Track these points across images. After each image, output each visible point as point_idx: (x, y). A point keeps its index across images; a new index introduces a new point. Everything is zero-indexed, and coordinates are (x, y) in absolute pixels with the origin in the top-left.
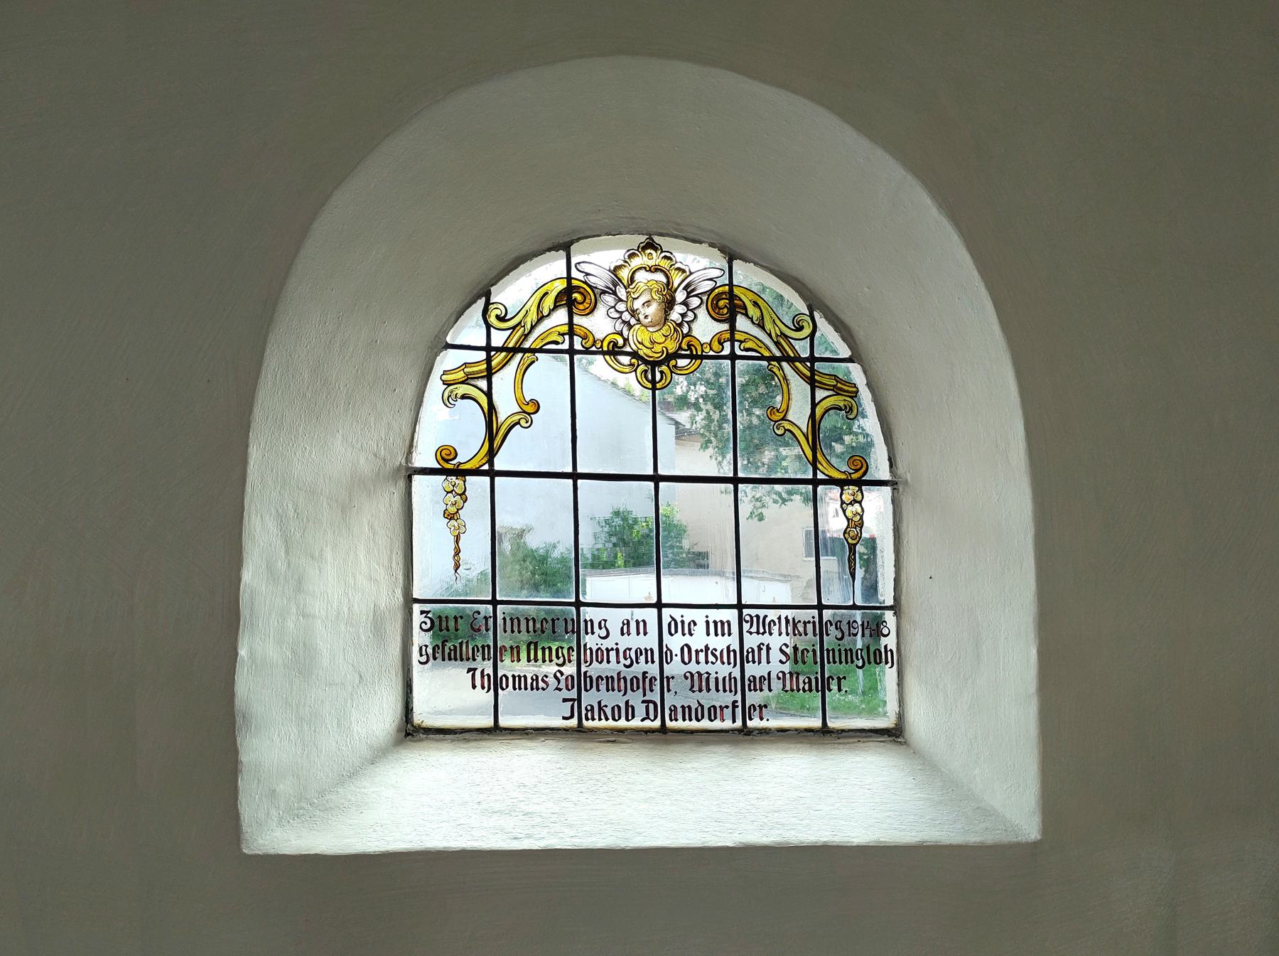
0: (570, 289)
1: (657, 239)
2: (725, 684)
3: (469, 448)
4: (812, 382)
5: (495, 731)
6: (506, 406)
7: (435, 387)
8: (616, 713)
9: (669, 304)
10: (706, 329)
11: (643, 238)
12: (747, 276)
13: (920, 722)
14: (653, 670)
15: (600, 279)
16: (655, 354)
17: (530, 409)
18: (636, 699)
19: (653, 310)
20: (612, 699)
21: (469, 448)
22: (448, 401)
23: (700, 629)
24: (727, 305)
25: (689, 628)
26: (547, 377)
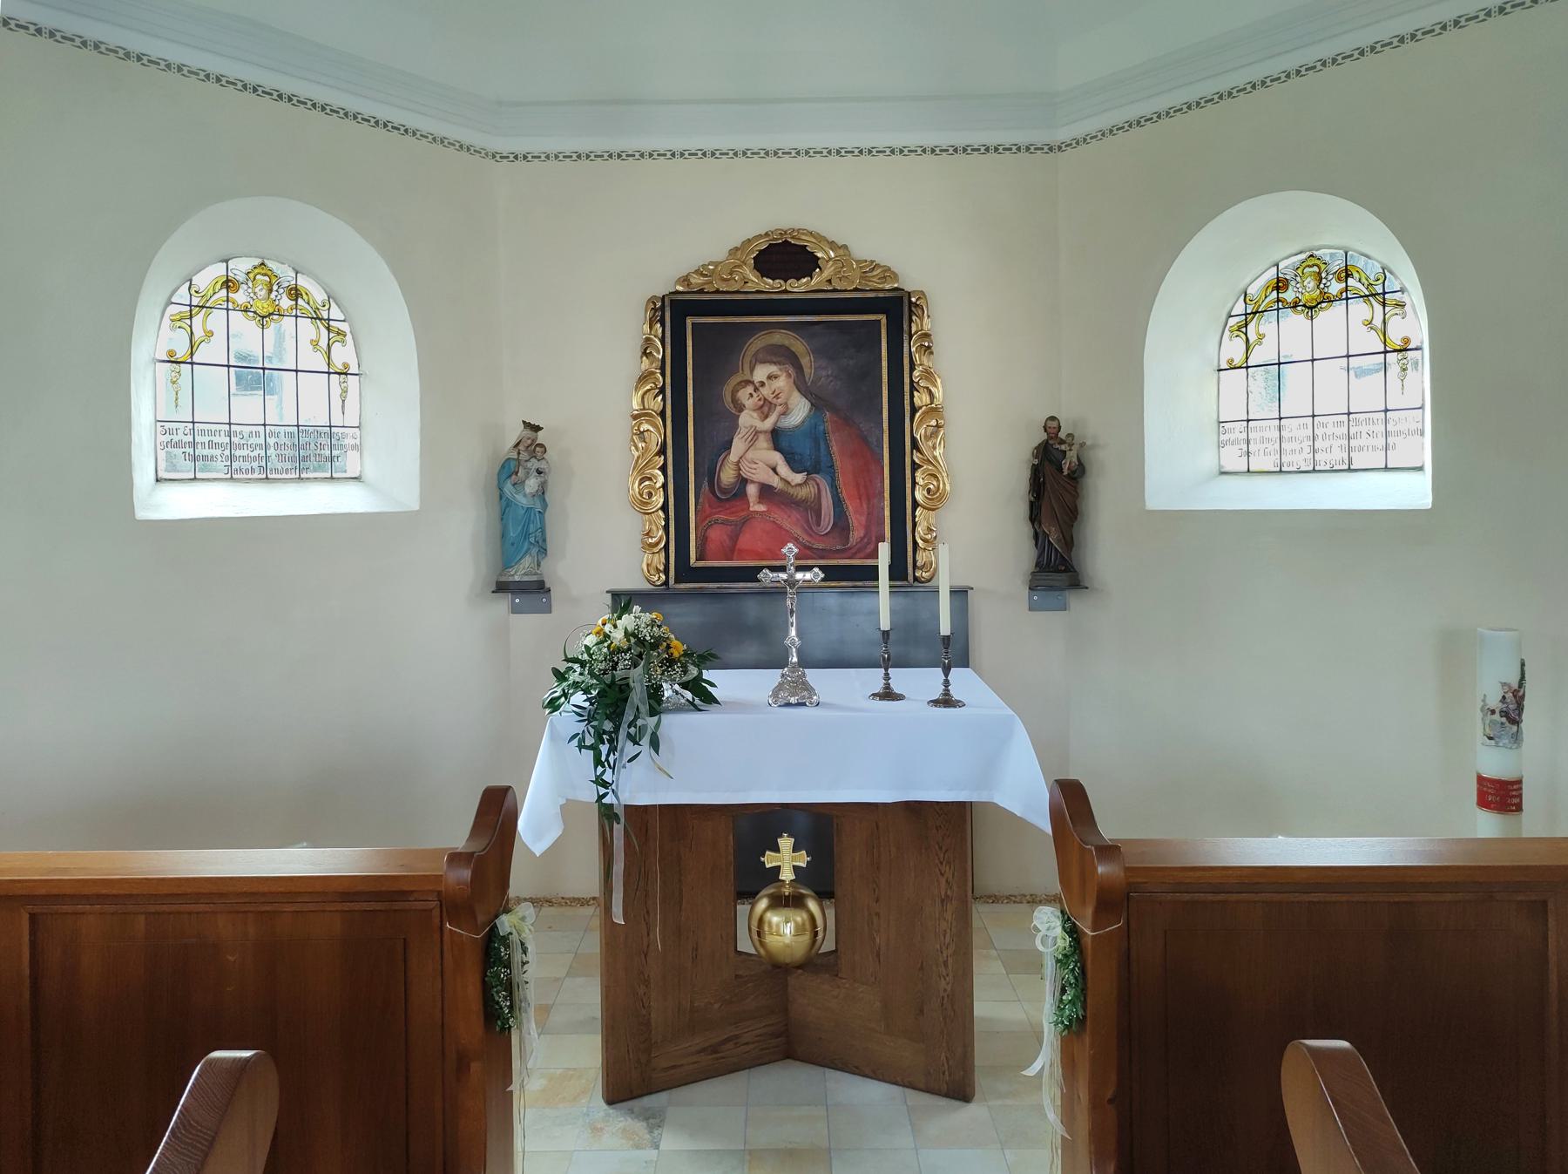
0: (228, 281)
1: (269, 264)
2: (291, 459)
3: (182, 352)
4: (328, 329)
5: (195, 479)
6: (199, 333)
7: (166, 321)
8: (247, 472)
9: (271, 291)
10: (286, 303)
11: (257, 262)
12: (304, 282)
13: (369, 473)
14: (262, 453)
15: (241, 277)
16: (264, 313)
17: (1261, 337)
18: (255, 465)
19: (264, 293)
20: (246, 465)
21: (182, 352)
22: (173, 329)
23: (1330, 426)
24: (295, 293)
25: (1324, 425)
26: (217, 319)
